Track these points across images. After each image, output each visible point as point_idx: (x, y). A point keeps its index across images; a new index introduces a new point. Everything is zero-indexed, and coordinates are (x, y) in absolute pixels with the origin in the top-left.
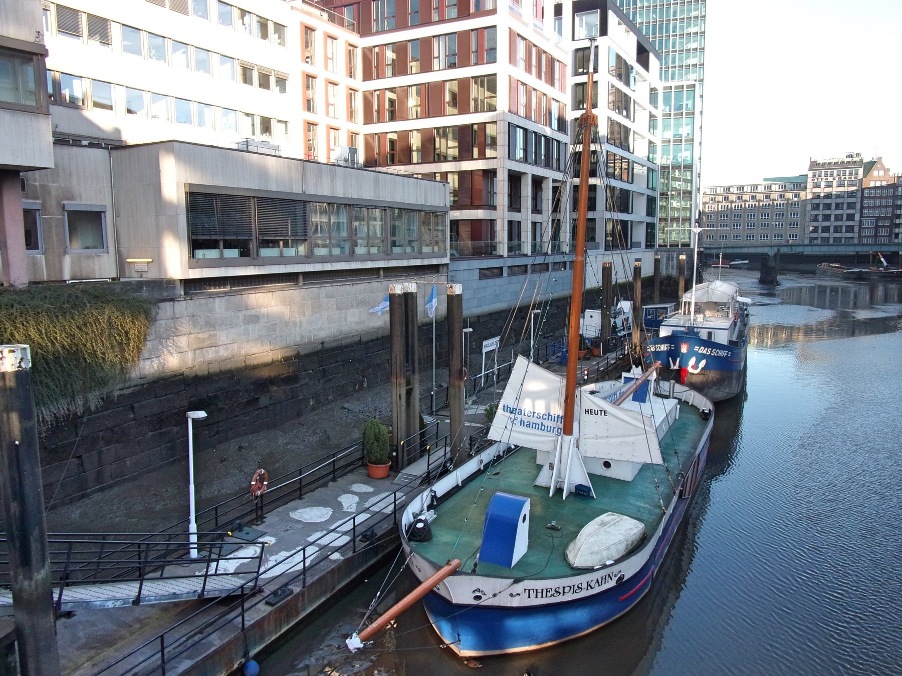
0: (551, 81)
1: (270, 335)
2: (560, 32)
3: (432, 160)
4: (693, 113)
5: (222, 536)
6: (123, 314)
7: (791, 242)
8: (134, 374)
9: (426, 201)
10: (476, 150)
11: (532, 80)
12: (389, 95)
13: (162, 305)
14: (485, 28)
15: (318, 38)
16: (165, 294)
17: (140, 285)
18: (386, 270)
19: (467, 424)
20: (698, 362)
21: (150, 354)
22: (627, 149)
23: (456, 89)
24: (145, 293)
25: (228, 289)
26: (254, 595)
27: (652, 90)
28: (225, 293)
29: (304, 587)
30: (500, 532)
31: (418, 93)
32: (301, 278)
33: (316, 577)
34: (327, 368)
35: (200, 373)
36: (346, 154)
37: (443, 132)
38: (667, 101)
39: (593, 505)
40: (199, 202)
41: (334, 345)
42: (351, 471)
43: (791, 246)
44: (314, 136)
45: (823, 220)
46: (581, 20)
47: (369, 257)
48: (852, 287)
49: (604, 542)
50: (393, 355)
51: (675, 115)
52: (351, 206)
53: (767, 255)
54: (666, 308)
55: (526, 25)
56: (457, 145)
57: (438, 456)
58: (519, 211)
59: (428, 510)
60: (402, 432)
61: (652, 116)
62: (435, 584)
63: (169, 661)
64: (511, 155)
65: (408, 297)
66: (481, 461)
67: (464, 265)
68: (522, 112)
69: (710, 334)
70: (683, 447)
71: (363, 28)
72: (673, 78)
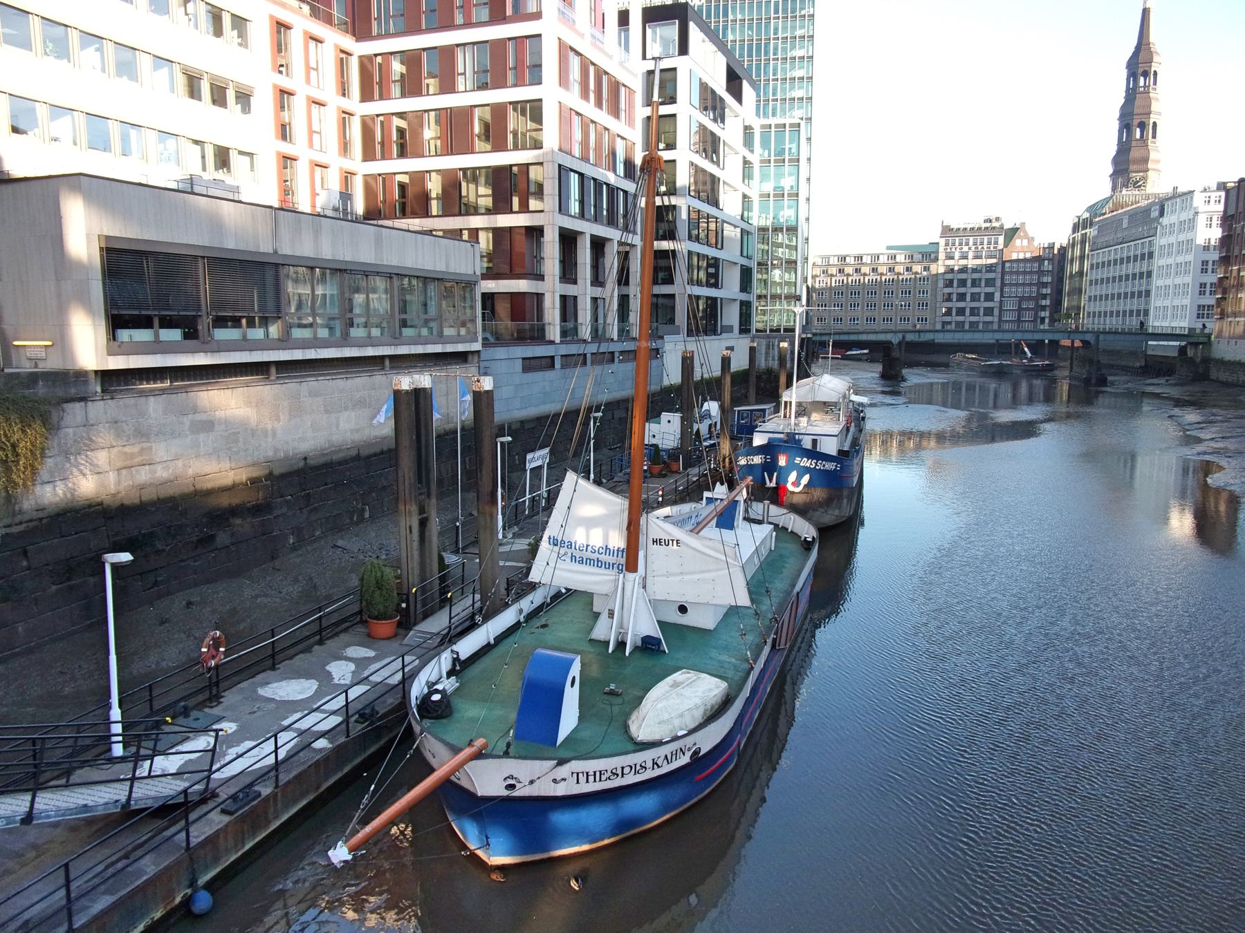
0: (615, 112)
1: (229, 449)
2: (627, 49)
3: (457, 211)
4: (798, 160)
5: (158, 725)
6: (7, 420)
7: (918, 327)
8: (27, 504)
9: (447, 266)
10: (516, 200)
11: (589, 109)
12: (397, 122)
13: (69, 407)
14: (527, 37)
15: (295, 39)
16: (73, 391)
17: (34, 378)
18: (393, 358)
19: (501, 563)
20: (799, 477)
21: (52, 475)
22: (715, 204)
23: (488, 117)
24: (41, 389)
25: (167, 384)
26: (203, 801)
27: (746, 128)
28: (163, 391)
29: (277, 786)
30: (541, 701)
31: (438, 122)
32: (273, 370)
33: (294, 773)
34: (313, 491)
35: (126, 502)
36: (336, 200)
37: (472, 175)
38: (765, 144)
39: (663, 660)
40: (120, 262)
41: (322, 460)
42: (345, 630)
43: (919, 331)
44: (292, 174)
45: (958, 300)
46: (654, 33)
47: (370, 342)
48: (992, 385)
49: (677, 708)
50: (400, 474)
51: (776, 161)
52: (339, 271)
53: (890, 343)
54: (764, 411)
55: (582, 35)
56: (490, 192)
57: (463, 607)
58: (575, 282)
59: (448, 677)
60: (414, 576)
61: (746, 162)
62: (453, 772)
63: (78, 898)
64: (562, 208)
65: (420, 396)
66: (521, 611)
67: (501, 352)
68: (577, 152)
69: (815, 442)
70: (779, 585)
71: (359, 27)
72: (774, 114)
